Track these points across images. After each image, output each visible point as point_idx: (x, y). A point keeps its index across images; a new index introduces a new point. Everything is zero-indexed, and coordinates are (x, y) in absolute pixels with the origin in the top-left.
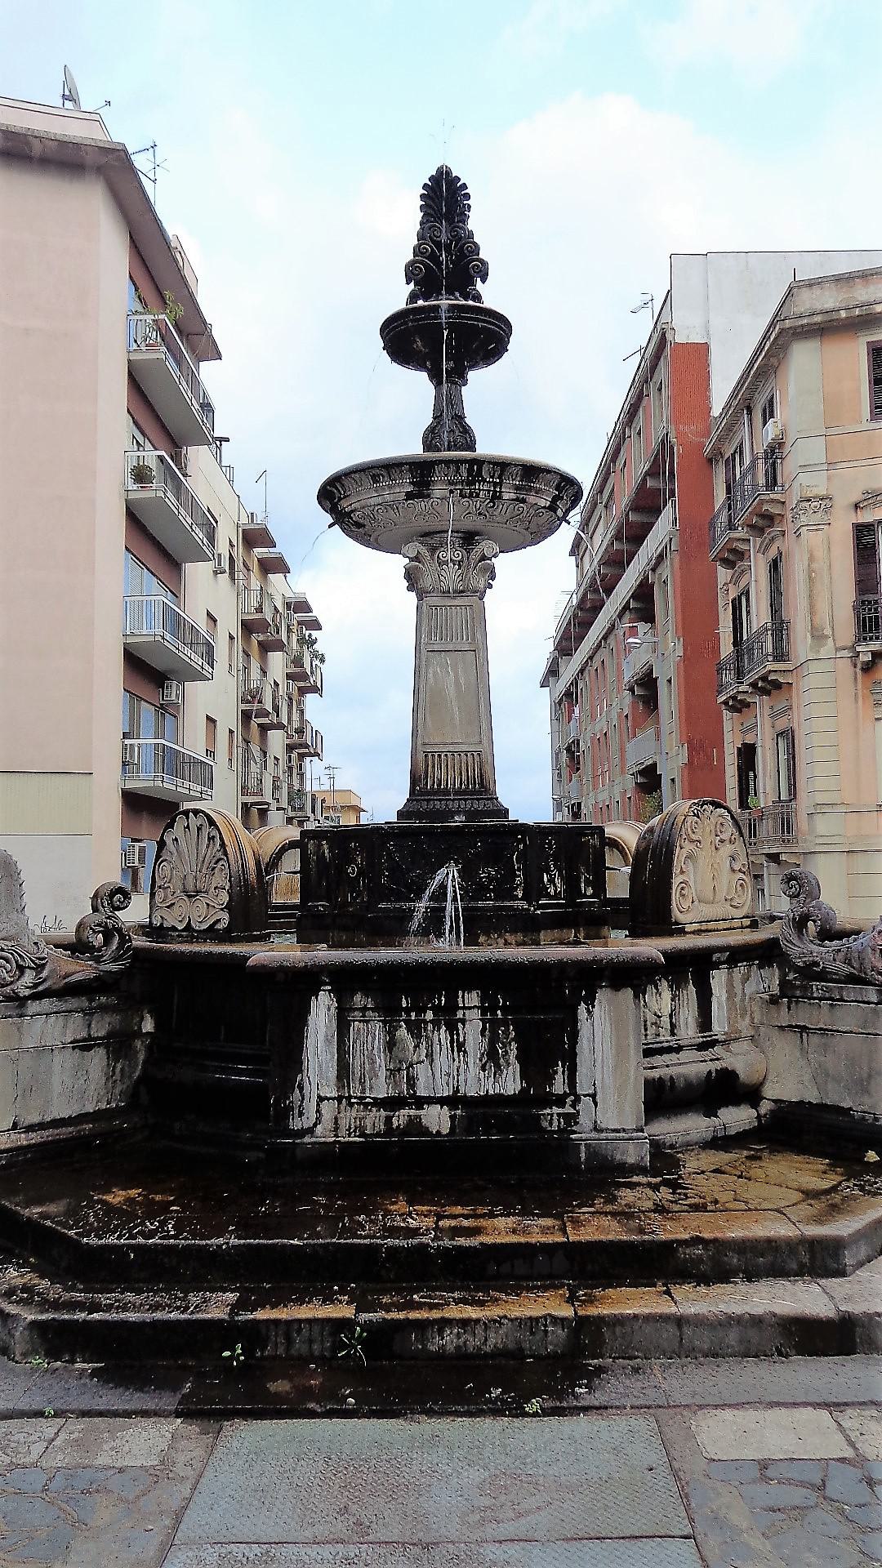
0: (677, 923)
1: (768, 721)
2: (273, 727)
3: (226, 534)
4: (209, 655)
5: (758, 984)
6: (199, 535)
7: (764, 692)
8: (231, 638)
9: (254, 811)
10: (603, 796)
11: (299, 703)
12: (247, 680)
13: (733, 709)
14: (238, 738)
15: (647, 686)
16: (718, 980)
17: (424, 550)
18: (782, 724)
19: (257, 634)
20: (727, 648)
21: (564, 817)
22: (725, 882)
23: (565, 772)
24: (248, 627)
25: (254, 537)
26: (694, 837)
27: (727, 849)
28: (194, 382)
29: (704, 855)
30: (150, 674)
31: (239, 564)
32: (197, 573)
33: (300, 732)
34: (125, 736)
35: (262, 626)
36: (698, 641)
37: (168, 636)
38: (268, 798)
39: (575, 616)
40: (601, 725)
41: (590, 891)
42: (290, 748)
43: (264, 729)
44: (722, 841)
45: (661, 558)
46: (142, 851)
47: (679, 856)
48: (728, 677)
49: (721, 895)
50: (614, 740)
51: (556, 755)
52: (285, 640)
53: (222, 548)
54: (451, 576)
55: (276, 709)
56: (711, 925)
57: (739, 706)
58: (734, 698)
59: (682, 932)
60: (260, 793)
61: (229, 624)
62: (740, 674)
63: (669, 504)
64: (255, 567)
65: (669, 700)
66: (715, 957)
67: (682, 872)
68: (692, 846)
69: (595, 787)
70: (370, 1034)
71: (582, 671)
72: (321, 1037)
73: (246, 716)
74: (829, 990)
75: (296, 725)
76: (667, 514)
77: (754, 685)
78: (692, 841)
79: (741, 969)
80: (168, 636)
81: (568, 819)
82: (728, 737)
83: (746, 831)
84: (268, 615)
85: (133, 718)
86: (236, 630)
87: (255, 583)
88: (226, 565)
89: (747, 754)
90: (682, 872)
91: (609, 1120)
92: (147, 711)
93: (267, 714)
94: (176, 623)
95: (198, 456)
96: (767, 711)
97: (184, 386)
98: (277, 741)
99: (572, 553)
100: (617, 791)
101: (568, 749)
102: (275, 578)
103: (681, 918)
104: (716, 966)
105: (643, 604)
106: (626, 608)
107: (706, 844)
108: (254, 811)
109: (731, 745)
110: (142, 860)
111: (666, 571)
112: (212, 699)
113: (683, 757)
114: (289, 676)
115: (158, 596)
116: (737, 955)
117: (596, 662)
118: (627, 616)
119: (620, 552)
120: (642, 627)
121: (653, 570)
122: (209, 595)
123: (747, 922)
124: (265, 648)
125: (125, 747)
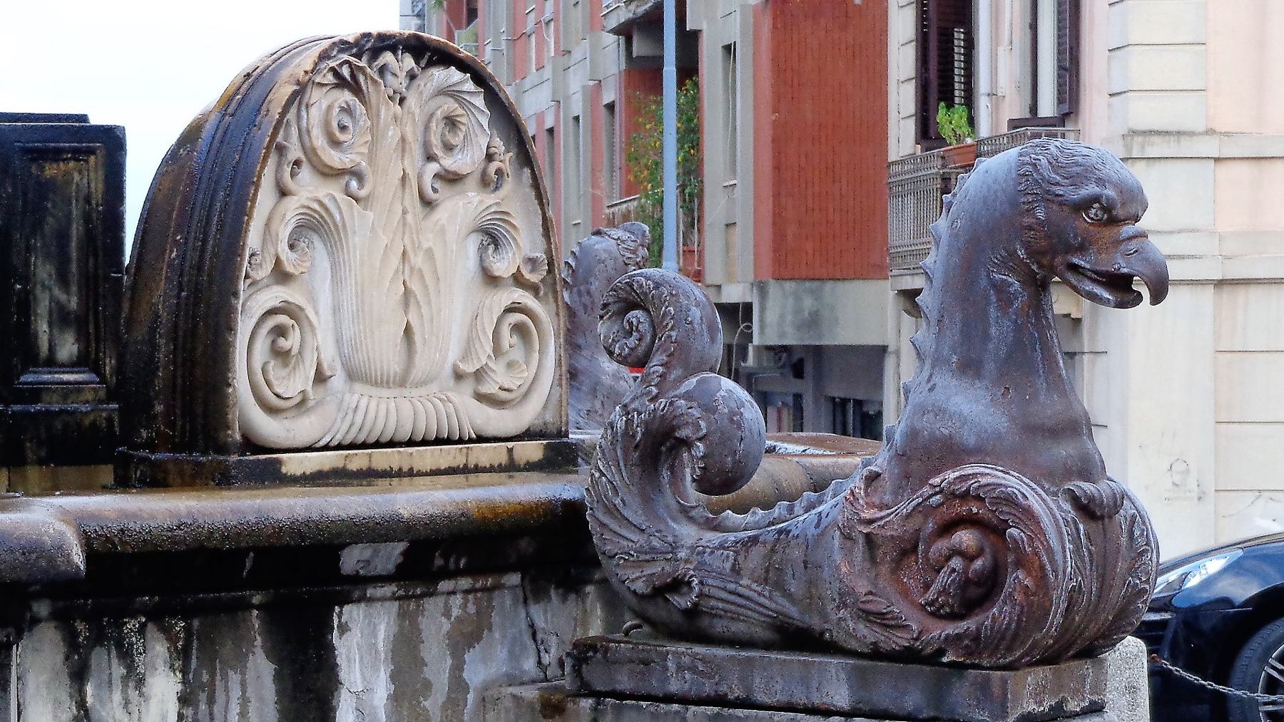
0: (251, 445)
5: (514, 656)
16: (362, 644)
21: (150, 626)
26: (334, 158)
27: (465, 207)
29: (370, 231)
41: (68, 348)
44: (451, 179)
47: (268, 224)
56: (383, 459)
59: (271, 476)
66: (351, 560)
67: (281, 275)
68: (329, 192)
74: (713, 668)
78: (328, 173)
79: (441, 614)
81: (150, 626)
90: (281, 275)
103: (270, 428)
104: (354, 588)
107: (383, 183)
116: (435, 556)
123: (532, 451)
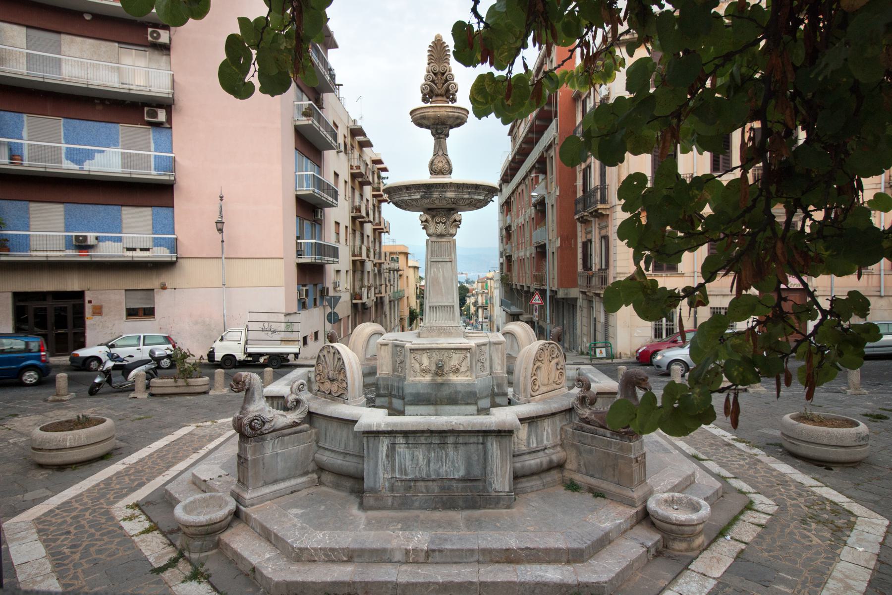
1: (597, 231)
2: (365, 222)
3: (342, 132)
4: (335, 194)
6: (330, 138)
7: (595, 217)
8: (346, 182)
9: (358, 263)
10: (521, 254)
11: (379, 207)
12: (353, 202)
13: (581, 222)
14: (350, 230)
15: (541, 205)
17: (429, 217)
18: (603, 233)
19: (358, 179)
20: (580, 194)
22: (553, 375)
23: (505, 240)
24: (354, 176)
25: (356, 132)
27: (554, 361)
28: (325, 63)
30: (309, 209)
31: (349, 146)
32: (329, 156)
33: (380, 224)
34: (298, 238)
35: (361, 175)
36: (568, 187)
37: (316, 191)
38: (364, 257)
39: (510, 165)
40: (521, 220)
42: (374, 230)
43: (362, 223)
45: (550, 146)
46: (307, 291)
48: (580, 207)
49: (551, 381)
50: (527, 228)
51: (501, 230)
52: (371, 180)
53: (341, 140)
54: (441, 228)
55: (367, 214)
57: (584, 221)
58: (582, 217)
60: (360, 255)
61: (345, 175)
62: (585, 208)
63: (554, 121)
64: (356, 145)
65: (552, 215)
69: (518, 249)
70: (402, 450)
71: (513, 193)
72: (384, 454)
73: (354, 219)
75: (377, 221)
76: (554, 124)
77: (591, 213)
80: (316, 191)
82: (579, 234)
83: (558, 387)
84: (363, 170)
85: (301, 228)
86: (348, 178)
87: (356, 153)
88: (342, 148)
89: (587, 245)
91: (498, 488)
92: (307, 224)
93: (363, 217)
94: (319, 183)
95: (328, 98)
96: (597, 226)
97: (321, 67)
98: (368, 228)
99: (509, 134)
100: (528, 253)
101: (506, 229)
102: (366, 150)
105: (541, 166)
106: (533, 167)
107: (546, 361)
108: (358, 263)
109: (581, 238)
110: (307, 295)
111: (552, 153)
112: (338, 214)
113: (558, 243)
114: (374, 196)
115: (310, 172)
117: (520, 190)
118: (534, 171)
119: (532, 138)
120: (541, 177)
121: (547, 151)
122: (336, 164)
124: (362, 184)
125: (297, 243)
